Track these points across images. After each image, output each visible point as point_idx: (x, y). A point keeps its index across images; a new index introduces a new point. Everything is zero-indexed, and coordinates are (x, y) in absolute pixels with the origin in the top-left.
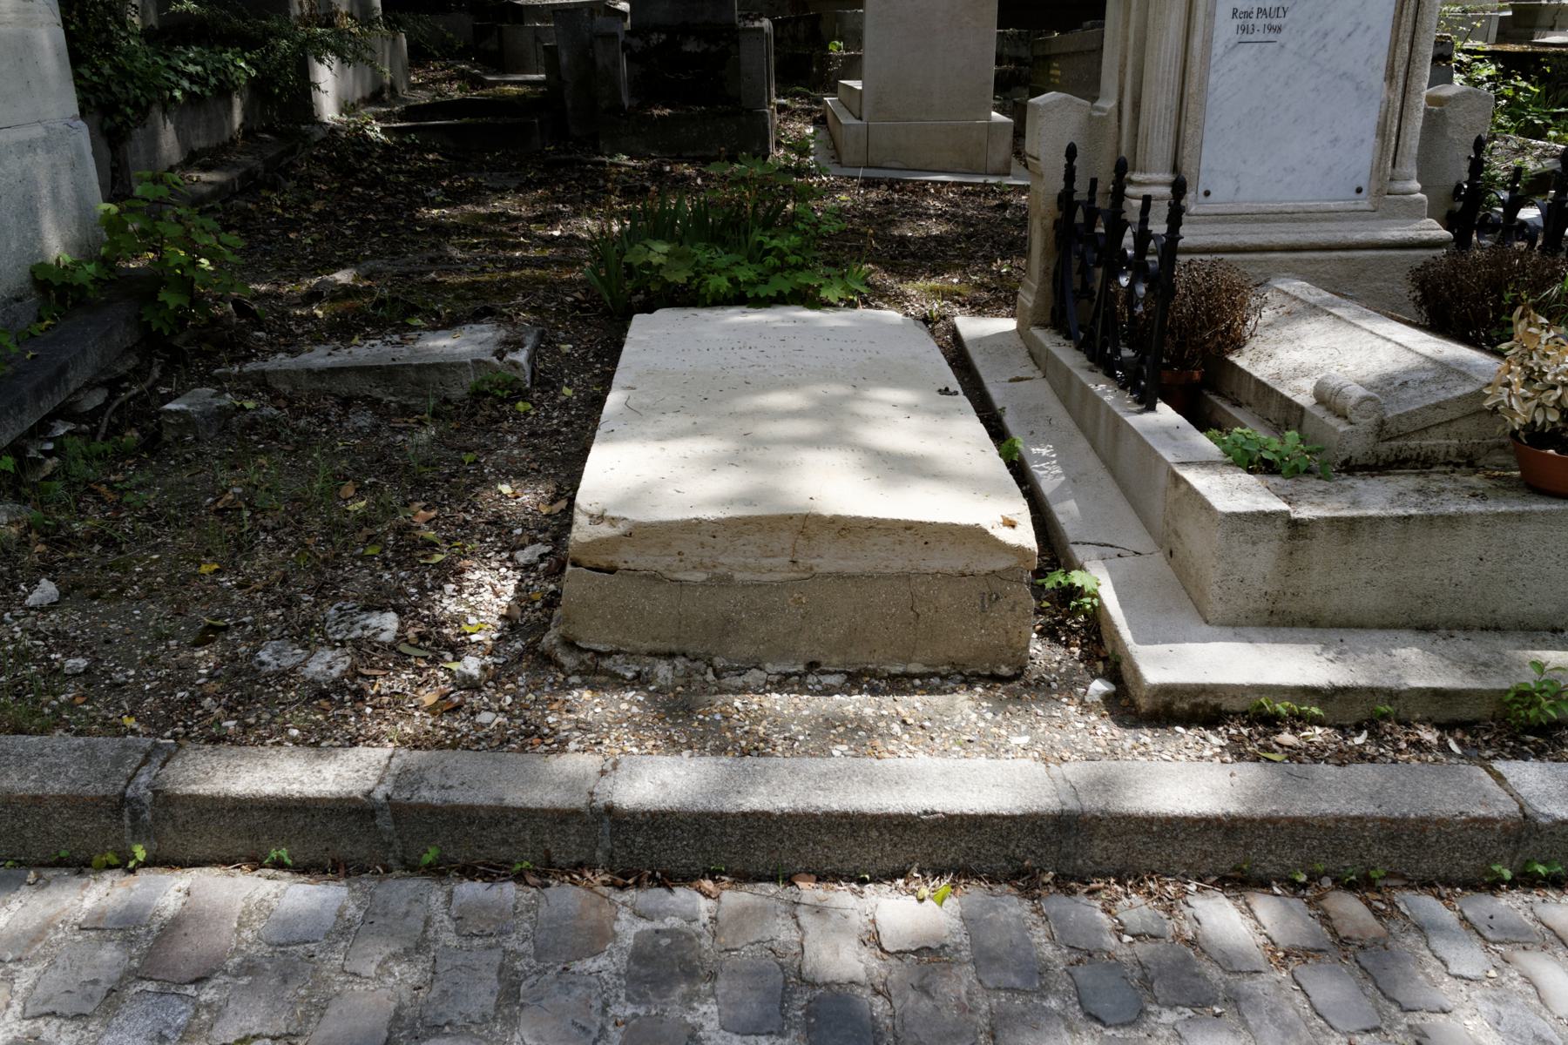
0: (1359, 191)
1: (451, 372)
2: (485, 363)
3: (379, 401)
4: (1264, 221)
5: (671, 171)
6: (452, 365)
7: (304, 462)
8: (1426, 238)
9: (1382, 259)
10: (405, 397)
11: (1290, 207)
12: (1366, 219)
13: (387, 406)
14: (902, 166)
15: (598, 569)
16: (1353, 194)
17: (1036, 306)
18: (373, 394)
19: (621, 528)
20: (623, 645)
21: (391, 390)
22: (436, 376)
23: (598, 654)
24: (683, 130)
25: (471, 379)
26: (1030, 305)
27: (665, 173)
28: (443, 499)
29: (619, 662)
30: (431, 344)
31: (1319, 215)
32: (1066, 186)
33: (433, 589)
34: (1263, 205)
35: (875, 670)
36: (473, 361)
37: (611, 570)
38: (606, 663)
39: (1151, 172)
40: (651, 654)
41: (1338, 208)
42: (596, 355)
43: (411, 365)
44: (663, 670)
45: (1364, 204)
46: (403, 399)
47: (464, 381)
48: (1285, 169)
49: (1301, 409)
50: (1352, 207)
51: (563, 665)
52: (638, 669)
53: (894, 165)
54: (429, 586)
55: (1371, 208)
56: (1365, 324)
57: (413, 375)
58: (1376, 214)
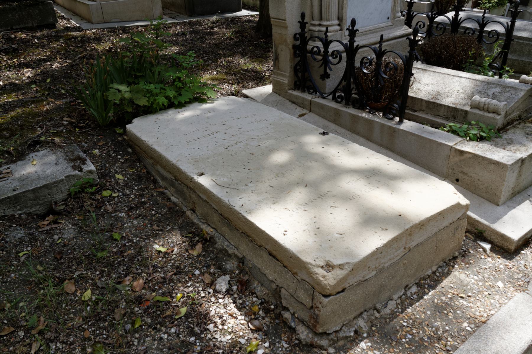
0: (388, 18)
1: (55, 187)
2: (73, 176)
3: (13, 216)
4: (366, 34)
5: (16, 37)
6: (54, 183)
7: (9, 276)
8: (407, 33)
9: (397, 42)
10: (29, 209)
11: (371, 28)
12: (391, 29)
13: (20, 218)
14: (119, 20)
15: (339, 293)
16: (387, 20)
17: (289, 82)
18: (7, 214)
19: (348, 269)
20: (344, 322)
21: (18, 208)
22: (46, 191)
23: (336, 332)
24: (10, 15)
25: (65, 188)
26: (286, 82)
27: (12, 38)
28: (137, 269)
29: (346, 330)
30: (24, 172)
31: (379, 29)
32: (302, 31)
33: (202, 333)
34: (364, 28)
35: (424, 277)
36: (66, 177)
37: (343, 291)
38: (341, 334)
39: (331, 21)
40: (354, 319)
41: (384, 26)
42: (114, 152)
43: (29, 190)
44: (361, 323)
45: (390, 24)
46: (27, 210)
47: (63, 189)
48: (370, 13)
49: (466, 112)
50: (387, 25)
51: (323, 346)
52: (354, 329)
53: (116, 20)
54: (199, 332)
55: (391, 24)
56: (431, 69)
57: (31, 196)
58: (393, 26)
